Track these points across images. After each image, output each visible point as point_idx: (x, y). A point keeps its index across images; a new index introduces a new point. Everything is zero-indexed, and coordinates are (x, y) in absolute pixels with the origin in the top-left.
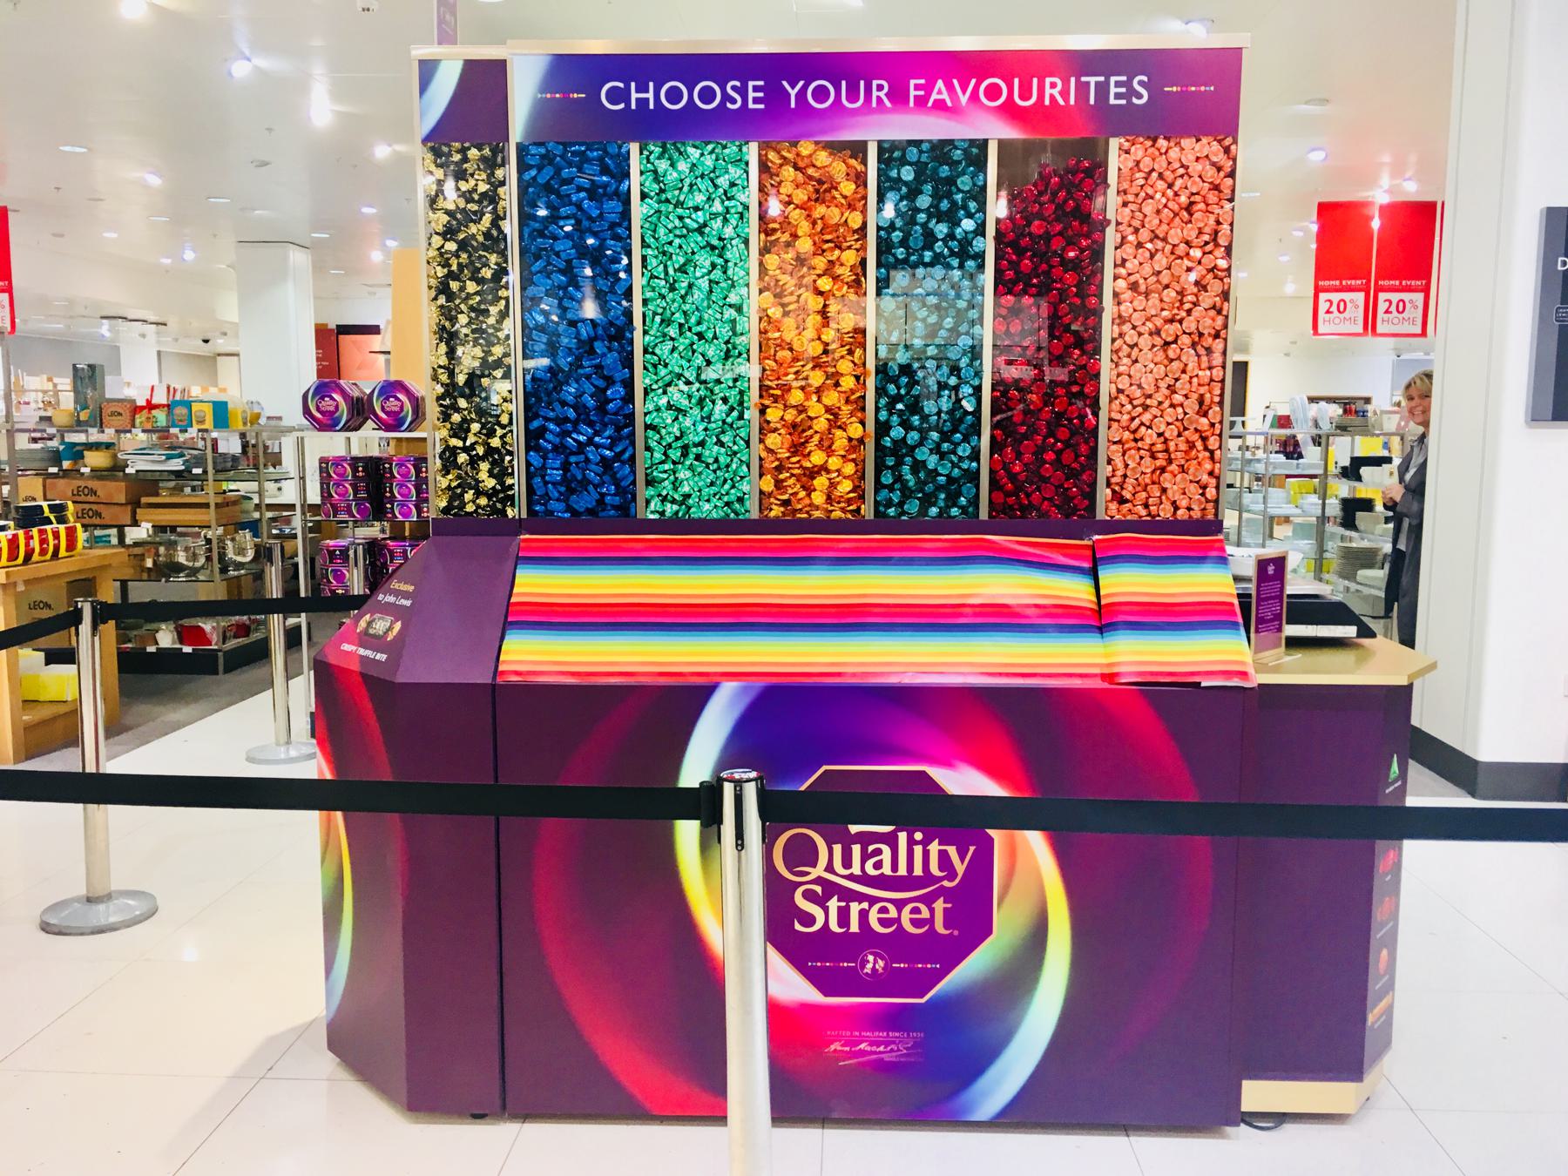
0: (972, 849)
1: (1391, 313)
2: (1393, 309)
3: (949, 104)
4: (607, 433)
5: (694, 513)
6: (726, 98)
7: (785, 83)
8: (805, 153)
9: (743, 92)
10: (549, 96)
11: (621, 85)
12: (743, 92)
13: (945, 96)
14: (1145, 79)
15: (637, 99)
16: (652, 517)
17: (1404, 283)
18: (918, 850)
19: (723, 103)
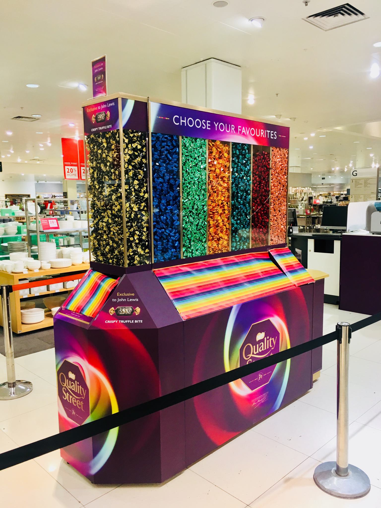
0: (276, 337)
1: (69, 172)
2: (69, 171)
3: (245, 134)
4: (173, 232)
5: (194, 255)
6: (202, 125)
7: (214, 123)
8: (218, 144)
9: (205, 123)
10: (160, 117)
11: (178, 117)
12: (205, 123)
13: (244, 132)
14: (209, 122)
15: (182, 122)
16: (184, 258)
17: (71, 163)
18: (268, 341)
19: (201, 127)
